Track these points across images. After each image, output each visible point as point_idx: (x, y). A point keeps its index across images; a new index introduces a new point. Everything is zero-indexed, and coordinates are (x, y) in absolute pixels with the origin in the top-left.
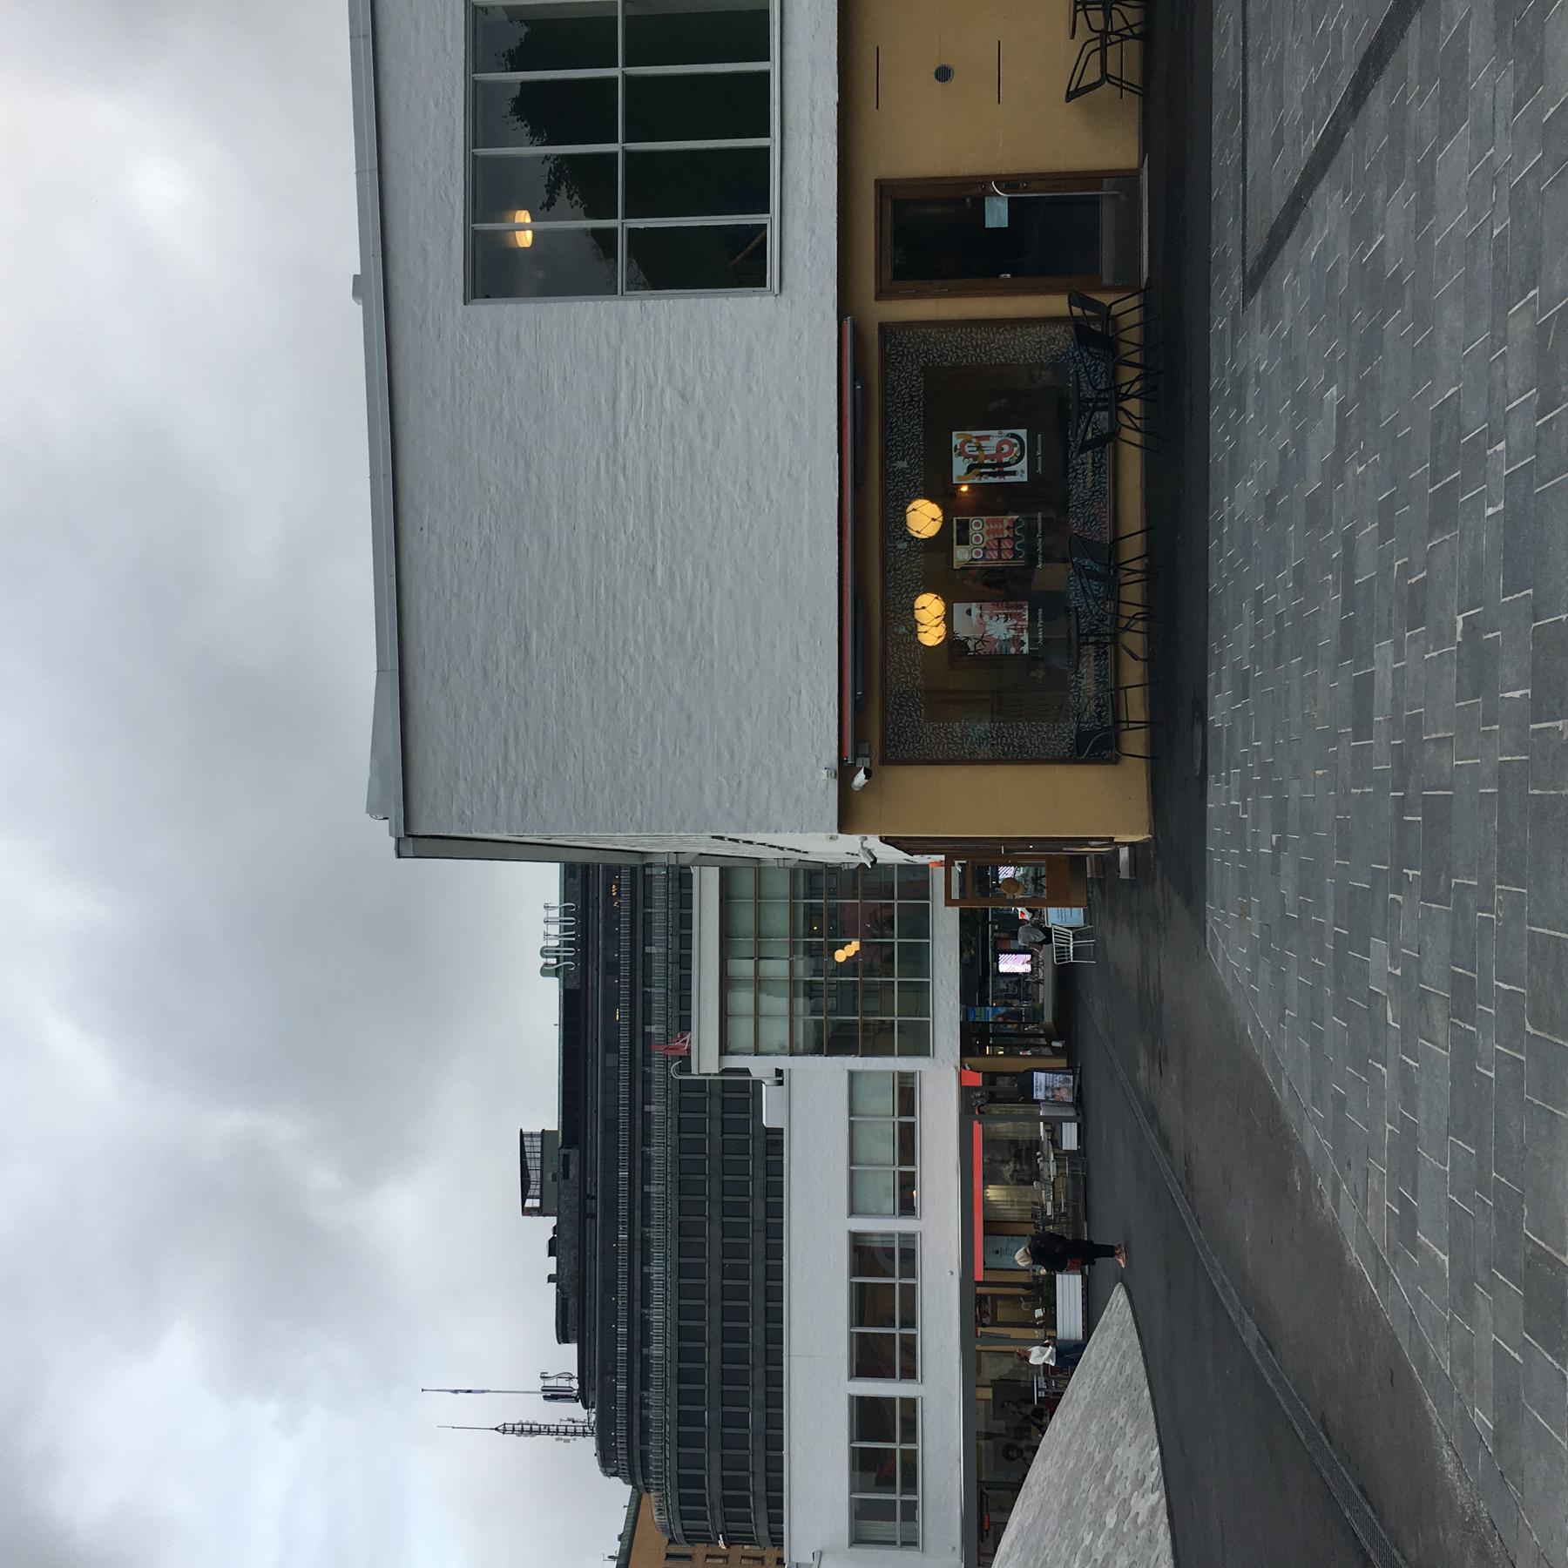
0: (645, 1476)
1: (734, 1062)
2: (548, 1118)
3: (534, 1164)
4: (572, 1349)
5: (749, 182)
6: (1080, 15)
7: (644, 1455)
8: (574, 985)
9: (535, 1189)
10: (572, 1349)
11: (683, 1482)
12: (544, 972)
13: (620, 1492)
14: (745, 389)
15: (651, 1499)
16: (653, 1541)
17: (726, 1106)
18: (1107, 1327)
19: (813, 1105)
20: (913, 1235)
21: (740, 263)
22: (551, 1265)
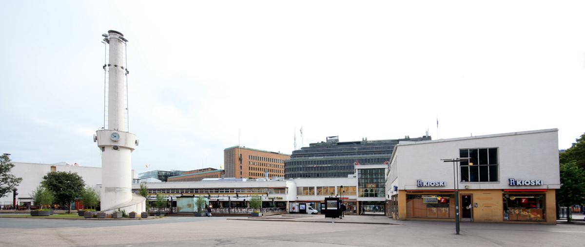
0: (293, 157)
1: (357, 170)
2: (341, 141)
3: (334, 138)
4: (309, 146)
5: (474, 179)
6: (366, 213)
7: (295, 157)
8: (362, 143)
9: (330, 138)
10: (309, 146)
11: (292, 162)
12: (363, 138)
13: (291, 153)
14: (449, 178)
15: (289, 158)
16: (285, 159)
17: (350, 166)
18: (268, 185)
19: (352, 181)
20: (494, 152)
21: (464, 178)
22: (320, 142)
